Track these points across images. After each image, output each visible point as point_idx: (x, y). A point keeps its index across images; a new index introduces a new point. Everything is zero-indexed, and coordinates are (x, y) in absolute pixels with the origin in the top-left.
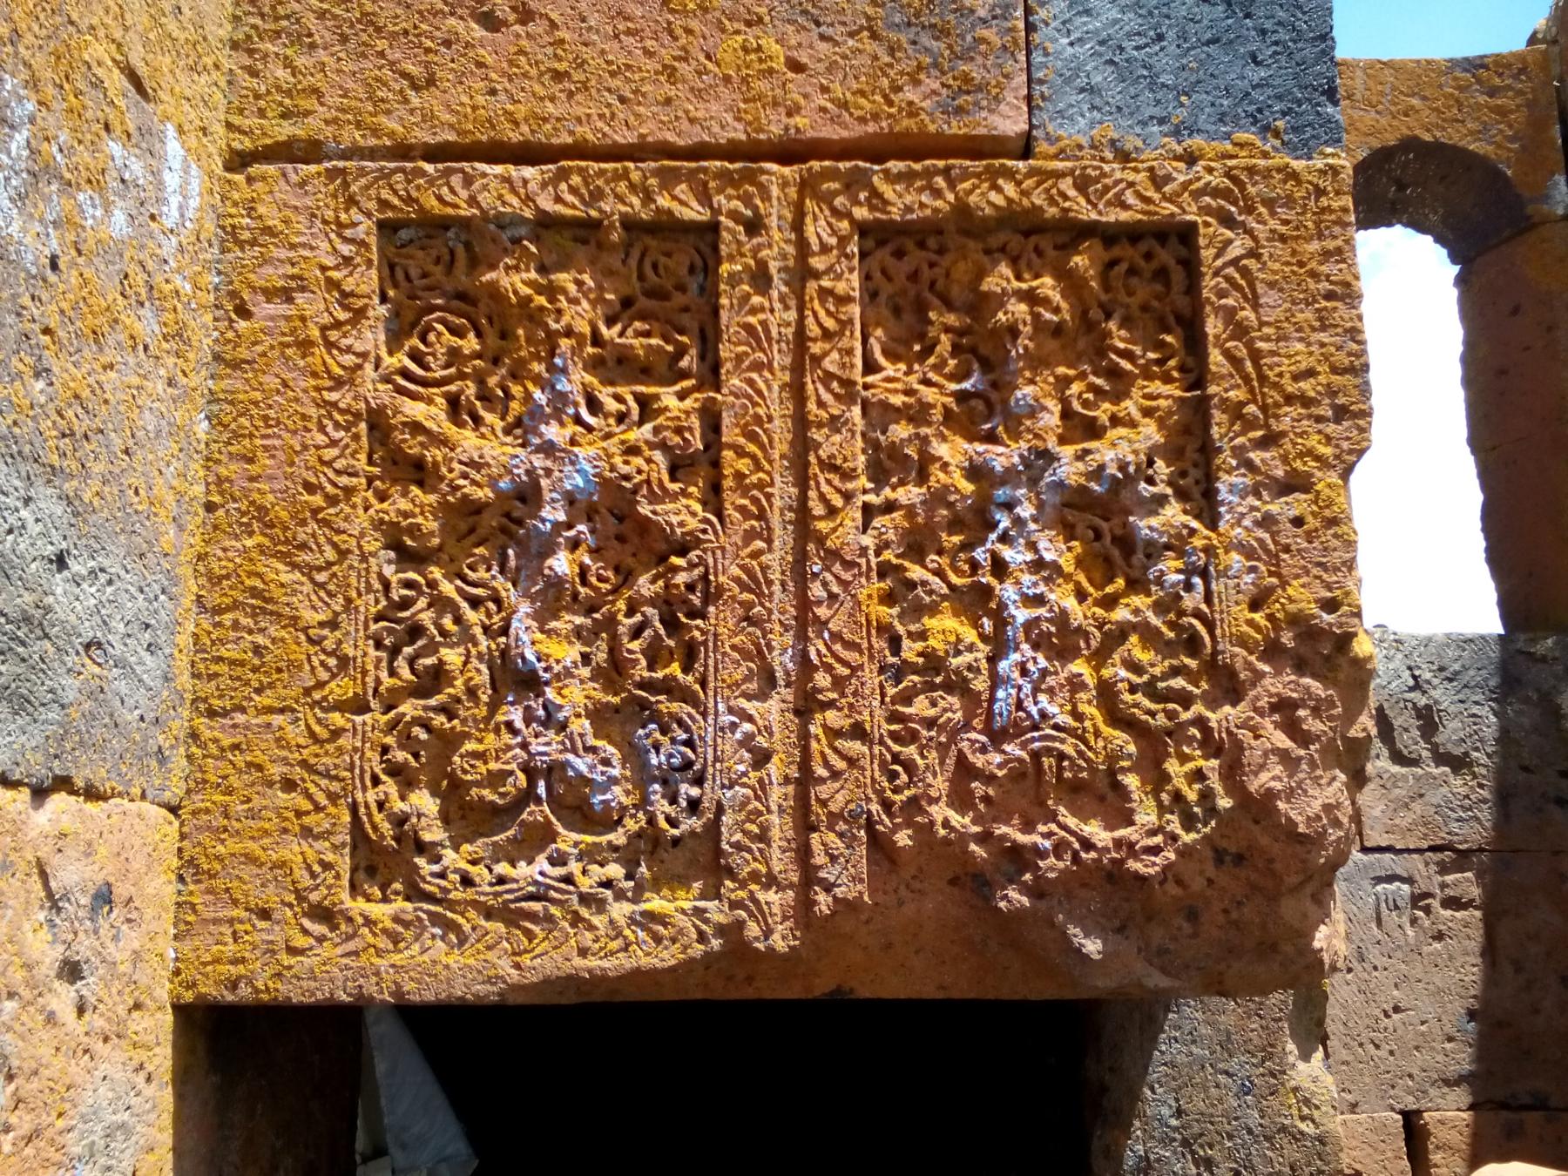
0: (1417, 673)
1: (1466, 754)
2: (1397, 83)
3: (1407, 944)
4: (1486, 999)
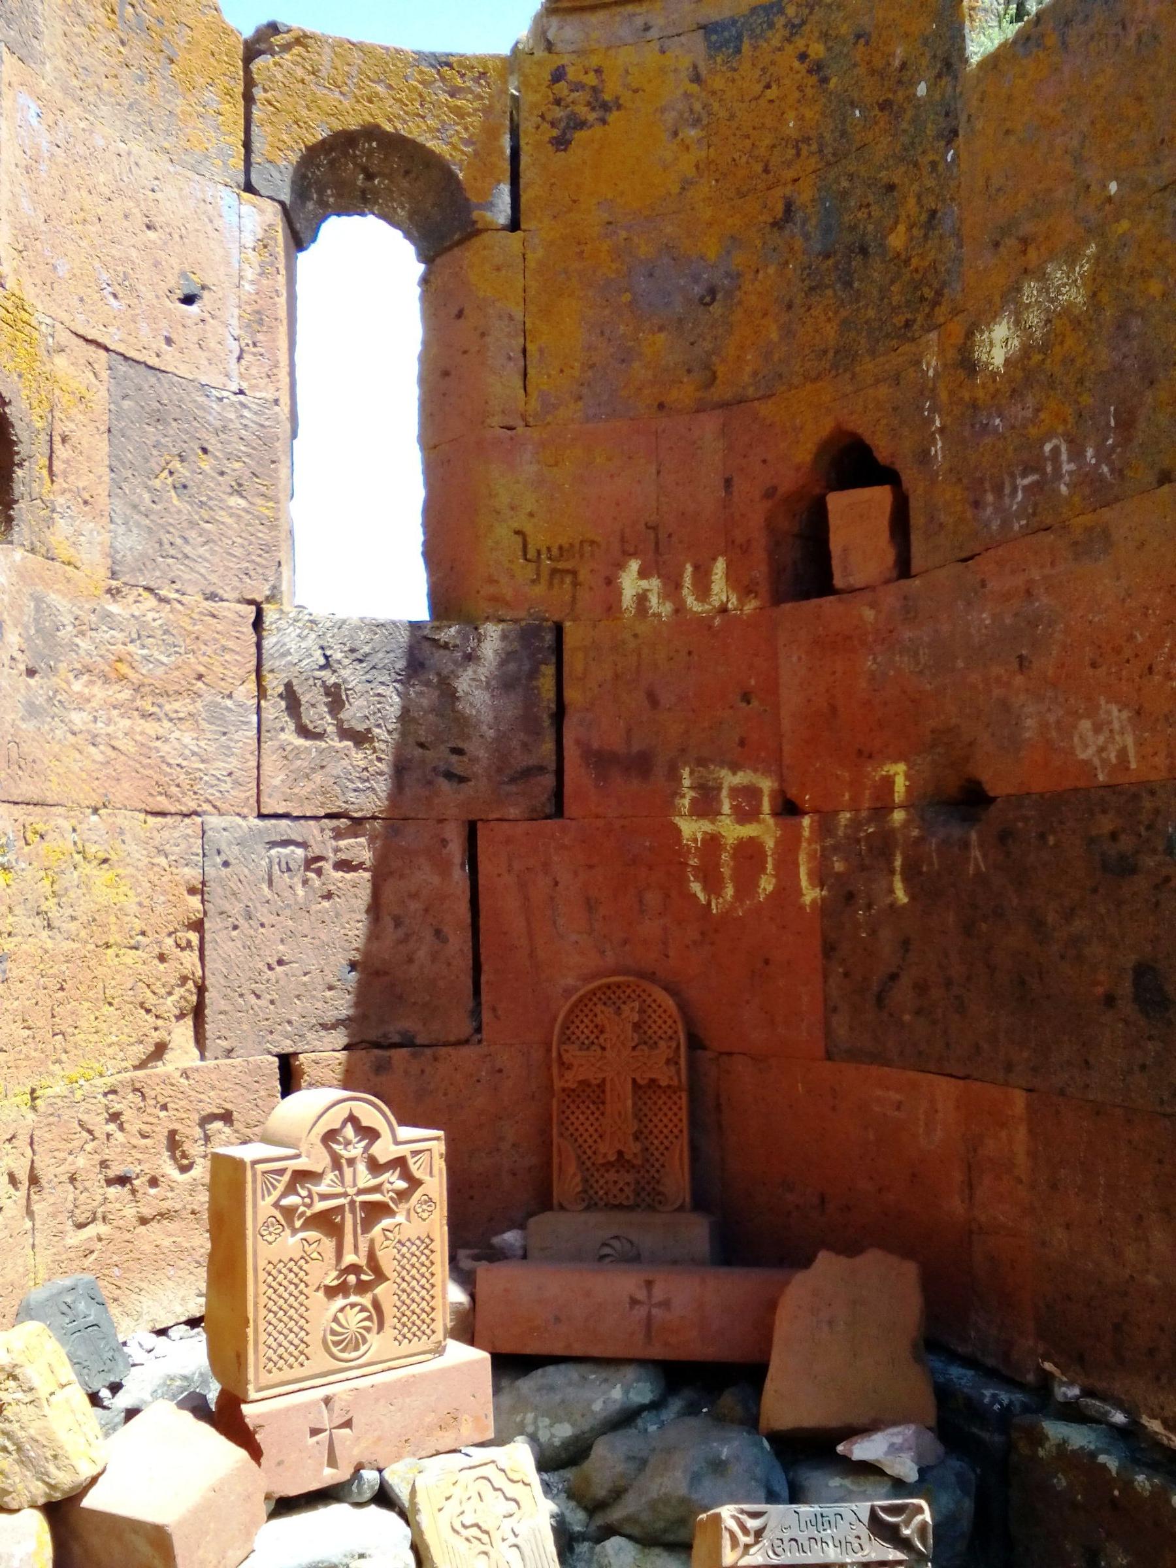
0: (328, 653)
1: (369, 730)
2: (364, 66)
3: (296, 902)
4: (367, 954)
